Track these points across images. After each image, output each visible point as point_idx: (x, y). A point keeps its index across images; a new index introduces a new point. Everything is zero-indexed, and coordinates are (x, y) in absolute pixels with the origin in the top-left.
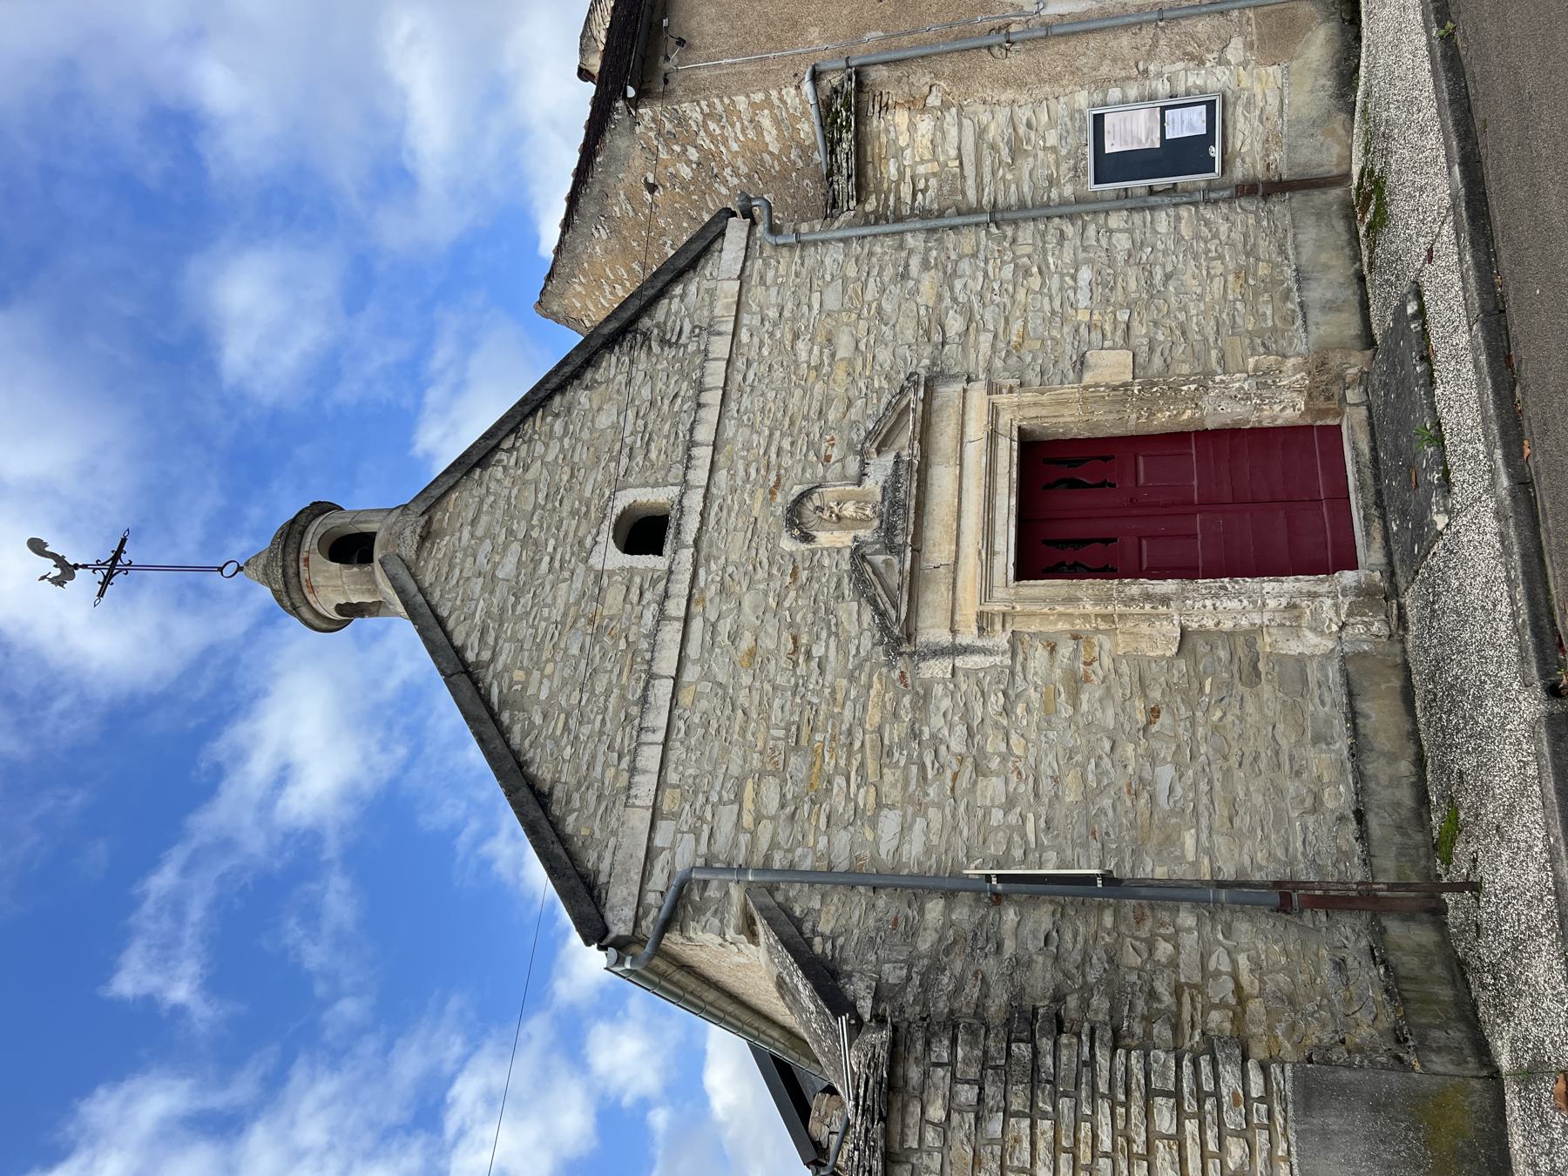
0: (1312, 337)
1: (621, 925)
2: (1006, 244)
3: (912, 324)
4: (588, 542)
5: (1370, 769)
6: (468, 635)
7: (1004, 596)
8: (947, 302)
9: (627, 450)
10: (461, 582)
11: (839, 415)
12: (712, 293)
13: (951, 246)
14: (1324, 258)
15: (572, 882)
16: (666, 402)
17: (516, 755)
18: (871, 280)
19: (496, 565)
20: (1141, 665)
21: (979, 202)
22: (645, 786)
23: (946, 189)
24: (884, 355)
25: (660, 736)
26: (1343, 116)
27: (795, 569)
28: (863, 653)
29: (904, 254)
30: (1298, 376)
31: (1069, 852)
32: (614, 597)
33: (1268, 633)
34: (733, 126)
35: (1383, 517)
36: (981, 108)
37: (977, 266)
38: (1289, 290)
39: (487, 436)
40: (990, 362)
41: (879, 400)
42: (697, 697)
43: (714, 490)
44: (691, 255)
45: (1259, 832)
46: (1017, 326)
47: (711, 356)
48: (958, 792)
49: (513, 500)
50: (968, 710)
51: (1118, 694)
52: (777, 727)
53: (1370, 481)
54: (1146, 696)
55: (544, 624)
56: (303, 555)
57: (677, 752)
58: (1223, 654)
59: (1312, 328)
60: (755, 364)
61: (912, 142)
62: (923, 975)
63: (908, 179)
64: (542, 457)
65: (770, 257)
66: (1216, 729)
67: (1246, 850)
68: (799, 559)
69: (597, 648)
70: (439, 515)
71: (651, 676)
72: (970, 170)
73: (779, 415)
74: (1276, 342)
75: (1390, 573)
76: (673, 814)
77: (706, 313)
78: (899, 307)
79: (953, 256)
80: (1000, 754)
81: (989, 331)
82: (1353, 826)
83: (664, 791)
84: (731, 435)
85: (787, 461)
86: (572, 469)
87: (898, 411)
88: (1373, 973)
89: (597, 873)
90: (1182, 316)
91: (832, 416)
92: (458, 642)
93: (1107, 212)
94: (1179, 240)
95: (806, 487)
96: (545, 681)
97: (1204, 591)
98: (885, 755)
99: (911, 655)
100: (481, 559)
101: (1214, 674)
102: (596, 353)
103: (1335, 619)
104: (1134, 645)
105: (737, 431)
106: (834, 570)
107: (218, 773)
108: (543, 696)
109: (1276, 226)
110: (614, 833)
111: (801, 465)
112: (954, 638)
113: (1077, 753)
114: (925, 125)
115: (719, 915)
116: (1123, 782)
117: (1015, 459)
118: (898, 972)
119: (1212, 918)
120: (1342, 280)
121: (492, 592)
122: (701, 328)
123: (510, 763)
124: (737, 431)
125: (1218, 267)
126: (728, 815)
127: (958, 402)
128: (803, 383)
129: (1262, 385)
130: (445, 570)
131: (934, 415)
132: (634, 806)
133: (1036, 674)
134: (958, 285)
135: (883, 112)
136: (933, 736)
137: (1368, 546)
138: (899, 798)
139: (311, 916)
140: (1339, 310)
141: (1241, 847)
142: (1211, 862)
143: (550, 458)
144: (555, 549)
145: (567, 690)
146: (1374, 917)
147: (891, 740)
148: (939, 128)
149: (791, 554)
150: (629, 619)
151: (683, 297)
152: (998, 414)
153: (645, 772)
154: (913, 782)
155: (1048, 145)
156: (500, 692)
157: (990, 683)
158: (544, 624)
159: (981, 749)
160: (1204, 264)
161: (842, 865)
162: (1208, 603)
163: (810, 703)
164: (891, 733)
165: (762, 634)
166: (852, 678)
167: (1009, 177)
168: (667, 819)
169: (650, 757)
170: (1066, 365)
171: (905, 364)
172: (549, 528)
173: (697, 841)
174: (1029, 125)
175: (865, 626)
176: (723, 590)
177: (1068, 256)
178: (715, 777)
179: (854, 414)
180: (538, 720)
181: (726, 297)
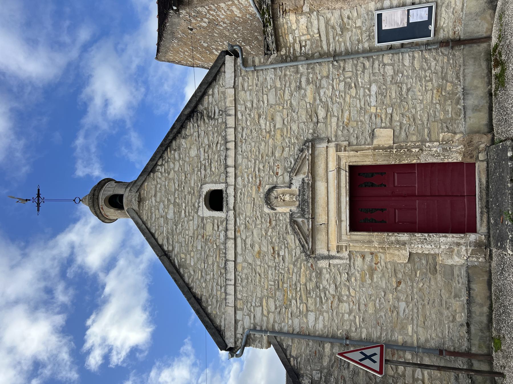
0: (467, 124)
1: (231, 344)
2: (341, 71)
3: (304, 113)
4: (196, 205)
5: (473, 309)
6: (163, 240)
7: (346, 239)
8: (318, 101)
9: (203, 167)
10: (156, 220)
11: (280, 155)
12: (224, 93)
13: (318, 72)
14: (476, 82)
15: (214, 330)
16: (214, 146)
17: (187, 285)
18: (287, 89)
19: (166, 213)
20: (394, 264)
21: (329, 50)
22: (231, 299)
23: (314, 46)
24: (294, 127)
25: (233, 282)
26: (490, 11)
27: (270, 220)
28: (297, 256)
29: (299, 76)
30: (460, 147)
31: (370, 330)
32: (209, 227)
33: (441, 256)
34: (221, 11)
35: (488, 212)
36: (327, 11)
37: (329, 83)
38: (460, 98)
39: (152, 160)
40: (336, 132)
41: (294, 149)
42: (243, 268)
43: (237, 186)
44: (213, 75)
45: (433, 328)
46: (346, 114)
47: (228, 126)
48: (333, 307)
49: (167, 187)
50: (335, 279)
51: (387, 275)
52: (271, 281)
53: (484, 197)
54: (396, 276)
55: (187, 237)
56: (100, 207)
57: (239, 288)
58: (424, 262)
59: (468, 120)
60: (245, 129)
61: (298, 27)
62: (325, 377)
63: (298, 42)
64: (174, 169)
65: (245, 76)
66: (420, 290)
67: (429, 333)
68: (271, 216)
69: (207, 247)
70: (142, 192)
71: (227, 261)
72: (324, 38)
73: (257, 153)
74: (452, 125)
75: (488, 236)
76: (241, 309)
77: (223, 104)
78: (299, 103)
79: (319, 78)
80: (346, 295)
81: (335, 116)
82: (465, 328)
83: (237, 301)
84: (240, 162)
85: (262, 174)
86: (185, 174)
87: (302, 159)
88: (467, 381)
89: (221, 326)
90: (413, 111)
91: (277, 155)
92: (160, 243)
93: (383, 55)
94: (414, 70)
95: (271, 186)
96: (192, 258)
97: (418, 240)
98: (308, 294)
99: (314, 258)
100: (161, 210)
101: (420, 269)
102: (184, 122)
103: (466, 255)
104: (393, 258)
105: (242, 160)
106: (284, 222)
107: (86, 105)
108: (192, 264)
109: (456, 63)
110: (223, 313)
111: (268, 176)
112: (329, 253)
113: (372, 296)
114: (303, 20)
115: (260, 343)
116: (388, 307)
117: (348, 180)
118: (317, 375)
119: (417, 355)
120: (482, 95)
121: (167, 224)
122: (222, 111)
123: (186, 289)
124: (242, 160)
125: (430, 87)
126: (259, 310)
127: (325, 153)
128: (264, 139)
129: (444, 150)
130: (150, 215)
131: (316, 158)
132: (228, 306)
133: (358, 267)
134: (322, 92)
135: (284, 15)
136: (324, 288)
137: (481, 225)
138: (314, 309)
139: (128, 145)
140: (480, 111)
141: (427, 332)
142: (417, 336)
143: (176, 169)
144: (185, 207)
145: (200, 262)
146: (469, 359)
147: (310, 288)
148: (310, 22)
149: (268, 214)
150: (215, 237)
151: (213, 95)
152: (340, 160)
153: (230, 295)
154: (318, 304)
155: (357, 26)
156: (178, 262)
157: (342, 269)
158: (187, 237)
159: (340, 293)
160: (424, 83)
161: (297, 330)
162: (420, 246)
163: (281, 273)
164: (309, 286)
165: (262, 245)
166: (294, 265)
167: (341, 40)
168: (239, 310)
169: (231, 289)
170: (367, 134)
171: (303, 132)
172: (181, 198)
173: (250, 319)
174: (349, 18)
175: (297, 245)
176: (246, 227)
177: (366, 79)
178: (253, 297)
179: (285, 154)
180: (192, 273)
181: (230, 97)
